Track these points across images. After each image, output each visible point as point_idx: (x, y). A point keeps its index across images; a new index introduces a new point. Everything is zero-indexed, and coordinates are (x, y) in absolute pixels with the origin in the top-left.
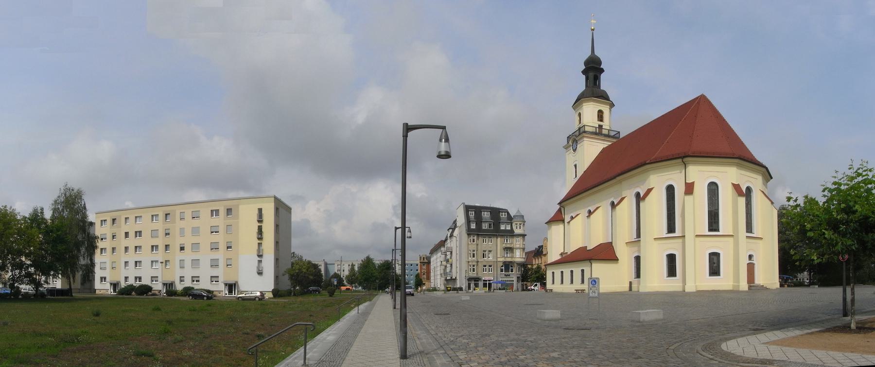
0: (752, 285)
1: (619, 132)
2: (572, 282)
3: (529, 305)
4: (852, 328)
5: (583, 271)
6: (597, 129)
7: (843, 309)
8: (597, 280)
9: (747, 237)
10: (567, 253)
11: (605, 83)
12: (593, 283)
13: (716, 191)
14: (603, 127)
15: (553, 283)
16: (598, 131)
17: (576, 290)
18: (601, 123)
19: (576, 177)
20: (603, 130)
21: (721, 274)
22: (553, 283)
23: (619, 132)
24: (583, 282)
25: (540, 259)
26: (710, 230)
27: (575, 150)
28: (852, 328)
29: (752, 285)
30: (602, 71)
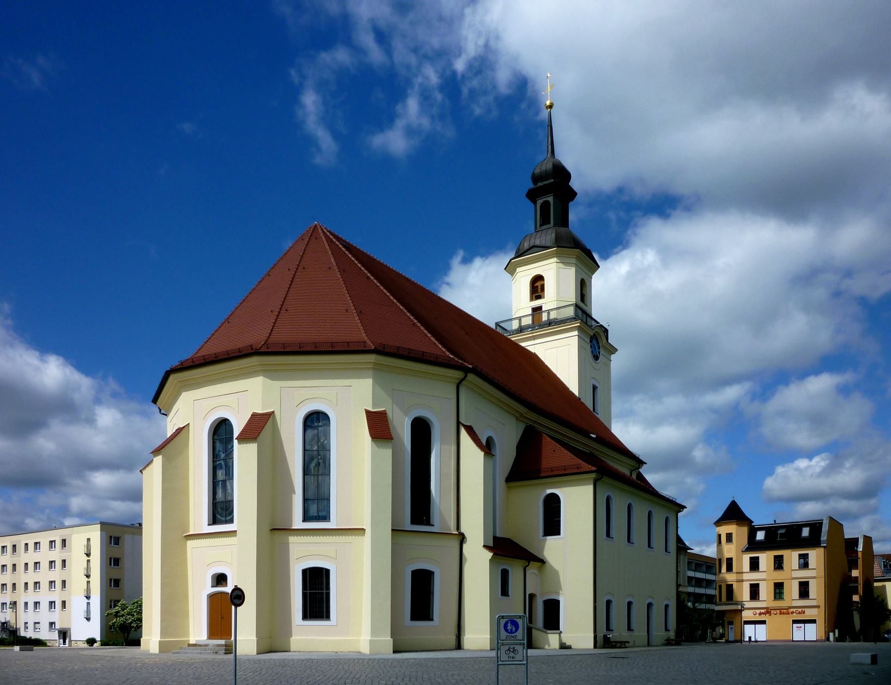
12: (509, 627)
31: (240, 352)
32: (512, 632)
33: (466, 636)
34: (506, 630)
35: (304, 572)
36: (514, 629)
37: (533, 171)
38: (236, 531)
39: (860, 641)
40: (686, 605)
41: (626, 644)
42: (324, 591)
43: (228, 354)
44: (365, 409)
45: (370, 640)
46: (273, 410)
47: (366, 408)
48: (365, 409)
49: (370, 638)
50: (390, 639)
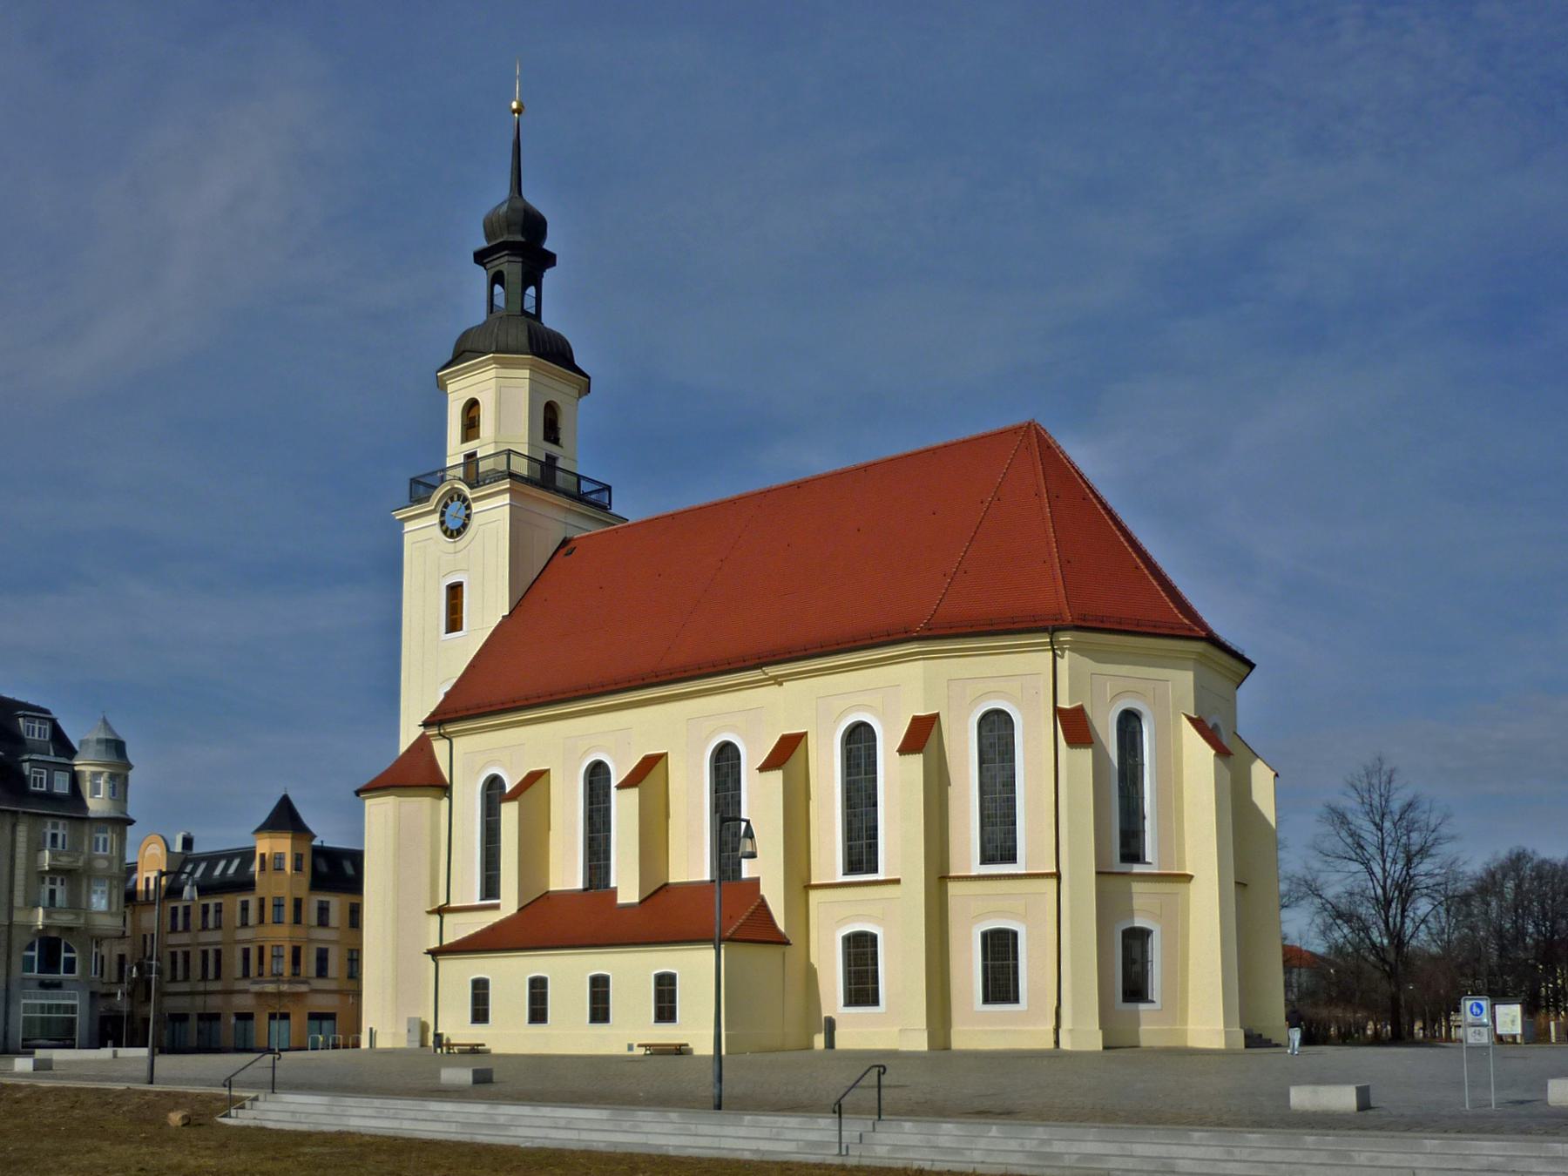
1: (609, 488)
9: (145, 936)
14: (560, 464)
19: (454, 623)
20: (559, 474)
23: (609, 488)
26: (986, 859)
32: (1477, 1015)
34: (1472, 1013)
36: (1479, 1012)
47: (443, 627)
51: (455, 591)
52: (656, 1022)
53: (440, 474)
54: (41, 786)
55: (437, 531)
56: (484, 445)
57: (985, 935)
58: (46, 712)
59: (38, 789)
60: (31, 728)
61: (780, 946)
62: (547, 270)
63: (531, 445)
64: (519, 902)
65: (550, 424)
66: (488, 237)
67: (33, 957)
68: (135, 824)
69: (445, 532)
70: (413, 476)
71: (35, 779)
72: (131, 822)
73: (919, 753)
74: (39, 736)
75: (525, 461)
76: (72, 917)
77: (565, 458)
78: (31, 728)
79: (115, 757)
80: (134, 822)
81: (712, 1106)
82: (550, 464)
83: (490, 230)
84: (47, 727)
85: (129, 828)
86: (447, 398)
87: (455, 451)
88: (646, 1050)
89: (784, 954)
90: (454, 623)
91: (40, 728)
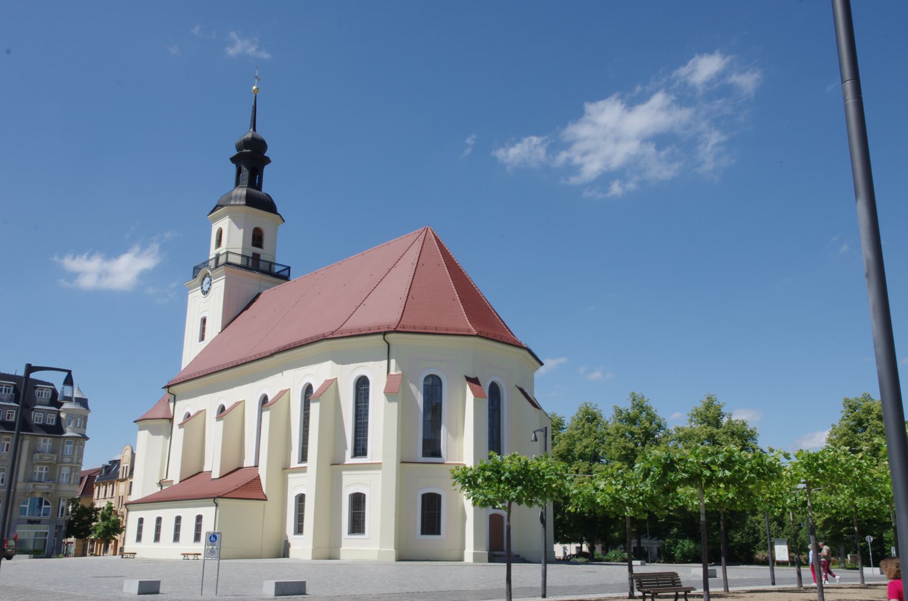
0: (496, 553)
1: (289, 268)
2: (176, 538)
3: (113, 577)
4: (893, 556)
5: (199, 518)
6: (250, 260)
7: (724, 579)
8: (217, 535)
9: (120, 497)
10: (172, 481)
11: (270, 185)
12: (212, 539)
13: (439, 388)
14: (262, 258)
15: (139, 538)
16: (250, 264)
17: (184, 554)
18: (257, 250)
19: (202, 338)
20: (261, 263)
21: (422, 536)
22: (139, 538)
23: (289, 268)
24: (197, 538)
25: (110, 488)
26: (425, 455)
27: (205, 293)
28: (893, 556)
29: (496, 553)
30: (267, 161)
31: (312, 339)
32: (213, 542)
33: (343, 548)
34: (211, 541)
35: (424, 496)
36: (214, 540)
37: (244, 206)
38: (381, 463)
39: (475, 548)
40: (858, 529)
41: (199, 556)
42: (437, 512)
43: (312, 339)
44: (200, 341)
45: (379, 551)
46: (335, 377)
47: (198, 341)
48: (200, 341)
49: (378, 549)
50: (393, 550)
51: (204, 321)
52: (154, 542)
53: (206, 264)
54: (40, 421)
55: (201, 293)
56: (222, 250)
57: (424, 496)
58: (52, 385)
59: (38, 423)
60: (47, 394)
61: (241, 500)
62: (265, 167)
63: (243, 248)
64: (180, 479)
65: (257, 238)
66: (238, 150)
67: (26, 508)
68: (89, 440)
69: (202, 292)
70: (195, 266)
71: (37, 418)
72: (87, 438)
73: (317, 402)
74: (45, 397)
75: (240, 257)
76: (47, 487)
77: (264, 254)
78: (47, 394)
79: (79, 406)
80: (89, 439)
81: (771, 583)
82: (256, 257)
83: (239, 147)
84: (50, 392)
85: (86, 442)
86: (211, 228)
87: (213, 252)
88: (185, 557)
89: (264, 506)
90: (202, 338)
91: (45, 393)
